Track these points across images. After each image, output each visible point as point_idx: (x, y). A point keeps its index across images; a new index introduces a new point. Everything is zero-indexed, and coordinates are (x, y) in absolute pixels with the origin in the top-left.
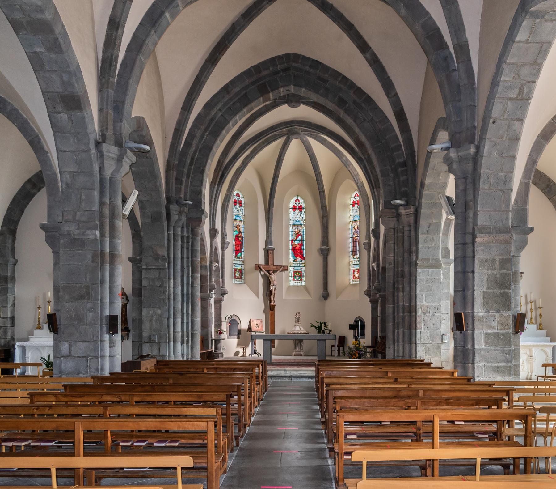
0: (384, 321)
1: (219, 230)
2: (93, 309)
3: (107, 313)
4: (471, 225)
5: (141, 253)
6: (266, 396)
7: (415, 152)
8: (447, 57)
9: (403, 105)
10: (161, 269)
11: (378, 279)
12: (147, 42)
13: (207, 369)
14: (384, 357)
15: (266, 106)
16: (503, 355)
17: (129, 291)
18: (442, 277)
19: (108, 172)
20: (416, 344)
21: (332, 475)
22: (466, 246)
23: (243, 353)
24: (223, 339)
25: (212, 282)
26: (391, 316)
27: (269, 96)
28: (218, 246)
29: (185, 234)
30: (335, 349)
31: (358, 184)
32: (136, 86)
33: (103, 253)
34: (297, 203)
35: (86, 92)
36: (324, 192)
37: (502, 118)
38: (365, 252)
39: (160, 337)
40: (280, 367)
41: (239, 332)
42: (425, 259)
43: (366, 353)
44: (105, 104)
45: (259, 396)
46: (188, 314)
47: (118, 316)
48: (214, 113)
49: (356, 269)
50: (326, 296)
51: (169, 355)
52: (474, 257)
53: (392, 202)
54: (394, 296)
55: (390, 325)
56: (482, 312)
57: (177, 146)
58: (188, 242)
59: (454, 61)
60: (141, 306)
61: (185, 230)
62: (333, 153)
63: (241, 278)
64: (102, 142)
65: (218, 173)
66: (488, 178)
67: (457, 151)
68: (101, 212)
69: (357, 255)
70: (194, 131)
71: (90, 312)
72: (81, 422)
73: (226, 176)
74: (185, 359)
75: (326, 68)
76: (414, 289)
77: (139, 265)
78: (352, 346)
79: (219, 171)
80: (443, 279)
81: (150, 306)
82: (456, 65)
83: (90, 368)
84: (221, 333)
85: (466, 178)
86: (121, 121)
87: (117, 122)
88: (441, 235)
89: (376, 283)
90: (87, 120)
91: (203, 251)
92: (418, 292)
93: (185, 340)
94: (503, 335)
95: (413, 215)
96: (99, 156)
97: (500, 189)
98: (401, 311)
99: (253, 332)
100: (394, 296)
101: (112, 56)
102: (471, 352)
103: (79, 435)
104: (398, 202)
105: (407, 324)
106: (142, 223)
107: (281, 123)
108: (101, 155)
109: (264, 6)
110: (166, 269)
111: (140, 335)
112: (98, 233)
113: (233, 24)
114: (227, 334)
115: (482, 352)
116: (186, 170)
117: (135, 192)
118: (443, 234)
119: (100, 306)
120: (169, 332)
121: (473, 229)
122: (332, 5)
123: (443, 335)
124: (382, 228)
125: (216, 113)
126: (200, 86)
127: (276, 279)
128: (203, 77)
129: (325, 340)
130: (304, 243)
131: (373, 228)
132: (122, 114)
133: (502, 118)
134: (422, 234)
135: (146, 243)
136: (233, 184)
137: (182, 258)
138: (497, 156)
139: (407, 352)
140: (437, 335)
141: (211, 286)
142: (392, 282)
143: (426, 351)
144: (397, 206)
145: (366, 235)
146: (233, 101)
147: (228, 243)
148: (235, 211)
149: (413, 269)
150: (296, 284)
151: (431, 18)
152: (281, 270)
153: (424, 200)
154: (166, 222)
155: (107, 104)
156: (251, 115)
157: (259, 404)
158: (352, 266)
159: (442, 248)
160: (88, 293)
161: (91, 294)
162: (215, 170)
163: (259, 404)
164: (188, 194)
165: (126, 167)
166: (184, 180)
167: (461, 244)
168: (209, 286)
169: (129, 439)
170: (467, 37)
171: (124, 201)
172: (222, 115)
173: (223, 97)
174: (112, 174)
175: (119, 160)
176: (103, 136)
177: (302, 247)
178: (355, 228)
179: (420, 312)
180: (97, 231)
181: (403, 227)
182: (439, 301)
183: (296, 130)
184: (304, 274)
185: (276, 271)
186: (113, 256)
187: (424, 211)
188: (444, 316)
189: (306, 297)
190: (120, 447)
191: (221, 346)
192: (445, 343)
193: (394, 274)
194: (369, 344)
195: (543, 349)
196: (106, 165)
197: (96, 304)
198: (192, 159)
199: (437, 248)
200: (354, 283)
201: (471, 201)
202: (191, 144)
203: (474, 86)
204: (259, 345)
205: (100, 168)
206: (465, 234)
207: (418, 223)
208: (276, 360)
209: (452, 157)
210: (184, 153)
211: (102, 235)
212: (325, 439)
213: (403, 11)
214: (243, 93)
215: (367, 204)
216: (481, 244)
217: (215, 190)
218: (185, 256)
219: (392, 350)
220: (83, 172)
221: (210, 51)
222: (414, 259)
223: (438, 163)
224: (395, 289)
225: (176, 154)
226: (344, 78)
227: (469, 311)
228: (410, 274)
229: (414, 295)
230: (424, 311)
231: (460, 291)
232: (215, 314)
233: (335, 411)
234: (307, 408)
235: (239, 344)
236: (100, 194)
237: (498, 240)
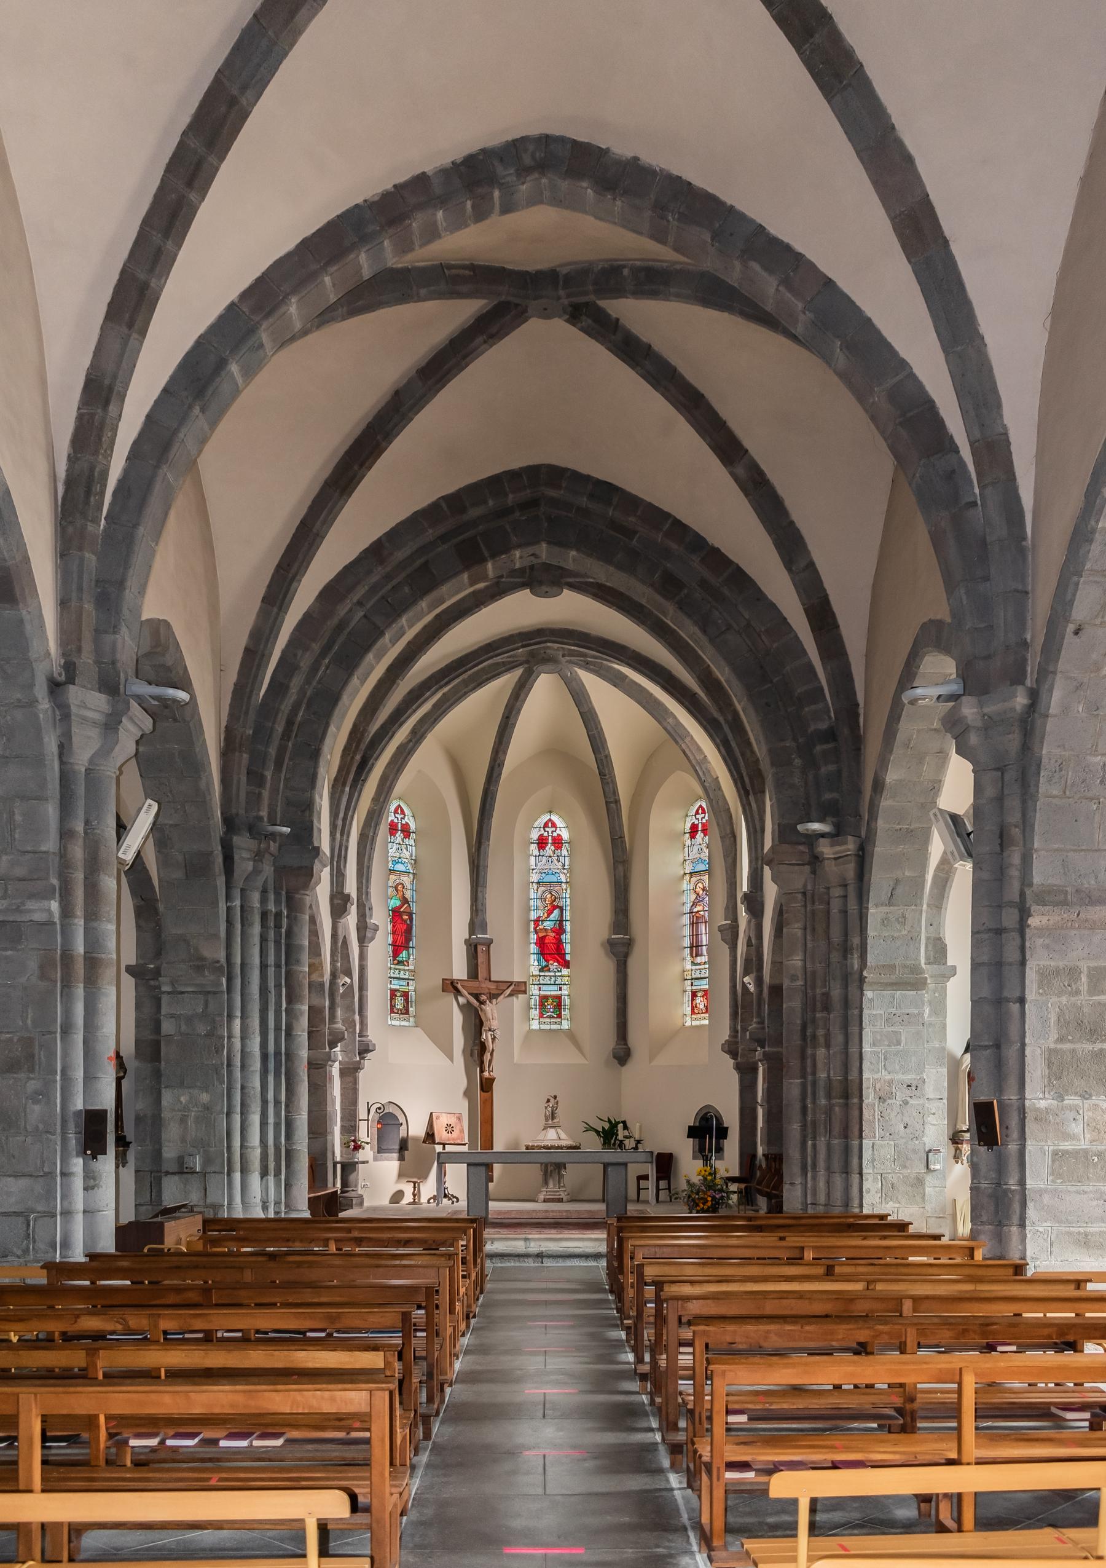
0: (775, 1117)
1: (354, 895)
2: (44, 1095)
3: (79, 1104)
4: (1016, 885)
5: (159, 953)
6: (482, 1306)
7: (858, 705)
8: (953, 472)
9: (828, 592)
10: (209, 992)
11: (759, 1015)
12: (181, 435)
13: (337, 1240)
14: (776, 1207)
15: (474, 593)
16: (1098, 1205)
17: (128, 1048)
18: (927, 1011)
19: (81, 758)
20: (861, 1174)
21: (685, 1517)
22: (1004, 936)
23: (414, 1195)
24: (363, 1163)
25: (337, 1023)
26: (797, 1106)
27: (486, 569)
28: (349, 934)
29: (271, 907)
30: (651, 1184)
31: (706, 784)
32: (153, 545)
33: (67, 958)
34: (550, 830)
35: (26, 560)
36: (617, 802)
37: (1098, 621)
38: (725, 949)
39: (207, 1161)
40: (512, 1231)
41: (403, 1145)
42: (884, 966)
43: (729, 1193)
44: (74, 587)
45: (469, 1306)
46: (277, 1102)
47: (105, 1111)
48: (345, 611)
49: (700, 990)
50: (622, 1055)
51: (230, 1204)
52: (1023, 963)
53: (799, 827)
54: (803, 1057)
55: (794, 1129)
56: (1044, 1098)
57: (251, 691)
58: (278, 926)
59: (971, 481)
60: (159, 1083)
61: (272, 897)
62: (644, 707)
63: (407, 1012)
64: (66, 683)
65: (353, 758)
66: (1061, 770)
67: (979, 701)
68: (63, 854)
69: (701, 955)
70: (295, 655)
71: (36, 1102)
72: (35, 1395)
73: (373, 764)
74: (271, 1215)
75: (631, 502)
76: (856, 1040)
77: (152, 983)
78: (696, 1179)
79: (355, 753)
80: (930, 1015)
81: (182, 1085)
82: (977, 491)
83: (34, 1242)
84: (357, 1148)
85: (1001, 770)
86: (115, 629)
87: (106, 632)
88: (925, 906)
89: (754, 1025)
90: (28, 627)
91: (315, 949)
92: (867, 1048)
93: (272, 1166)
95: (853, 858)
96: (58, 718)
97: (1090, 794)
98: (821, 1093)
99: (439, 1144)
100: (803, 1057)
101: (92, 469)
102: (1017, 1197)
103: (30, 1427)
104: (816, 826)
105: (837, 1128)
106: (160, 880)
107: (512, 636)
108: (63, 714)
109: (471, 353)
110: (223, 992)
111: (157, 1155)
112: (55, 906)
113: (397, 393)
114: (371, 1149)
115: (1046, 1199)
116: (272, 751)
117: (150, 805)
118: (928, 905)
119: (62, 1089)
120: (229, 1147)
121: (1022, 894)
122: (650, 346)
123: (930, 1151)
124: (771, 892)
125: (351, 610)
126: (311, 545)
127: (496, 1015)
128: (318, 523)
129: (625, 1165)
130: (568, 927)
131: (745, 888)
132: (118, 612)
133: (1098, 621)
134: (877, 906)
135: (172, 929)
136: (388, 784)
137: (264, 967)
138: (1084, 715)
139: (838, 1195)
140: (914, 1151)
141: (332, 1032)
142: (799, 1022)
143: (888, 1191)
144: (812, 839)
145: (727, 908)
146: (394, 582)
147: (376, 928)
148: (392, 850)
149: (853, 989)
150: (547, 1027)
151: (912, 376)
152: (508, 992)
153: (881, 824)
154: (223, 878)
155: (80, 589)
156: (438, 616)
157: (468, 1327)
158: (689, 982)
159: (928, 939)
160: (31, 1056)
161: (37, 1057)
162: (344, 751)
163: (468, 1327)
164: (279, 808)
165: (126, 744)
166: (268, 774)
167: (990, 930)
168: (330, 1034)
169: (155, 1430)
170: (1005, 422)
171: (122, 828)
172: (365, 616)
173: (369, 572)
174: (91, 761)
175: (111, 725)
176: (70, 668)
177: (563, 937)
178: (698, 889)
179: (872, 1096)
180: (52, 902)
181: (828, 888)
182: (920, 1068)
183: (548, 651)
184: (568, 1002)
185: (496, 996)
186: (93, 963)
187: (881, 850)
188: (933, 1106)
189: (569, 1057)
190: (129, 1451)
191: (357, 1180)
192: (935, 1171)
193: (805, 1005)
194: (735, 1172)
196: (75, 740)
197: (49, 1083)
198: (290, 723)
199: (914, 939)
200: (695, 1023)
201: (1016, 826)
202: (287, 687)
203: (1024, 543)
204: (457, 1177)
205: (61, 747)
206: (1000, 906)
207: (866, 879)
208: (500, 1212)
209: (966, 717)
210: (267, 710)
211: (67, 912)
212: (651, 1418)
213: (841, 359)
214: (419, 563)
215: (728, 831)
216: (1041, 931)
217: (345, 799)
218: (271, 960)
219: (798, 1191)
220: (17, 757)
221: (336, 460)
222: (856, 966)
223: (919, 731)
224: (807, 1039)
225: (247, 713)
226: (678, 523)
227: (1011, 1096)
228: (846, 1003)
229: (857, 1055)
230: (881, 1094)
231: (986, 1047)
232: (342, 1102)
234: (593, 1336)
235: (401, 1175)
236: (61, 811)
237: (1087, 920)
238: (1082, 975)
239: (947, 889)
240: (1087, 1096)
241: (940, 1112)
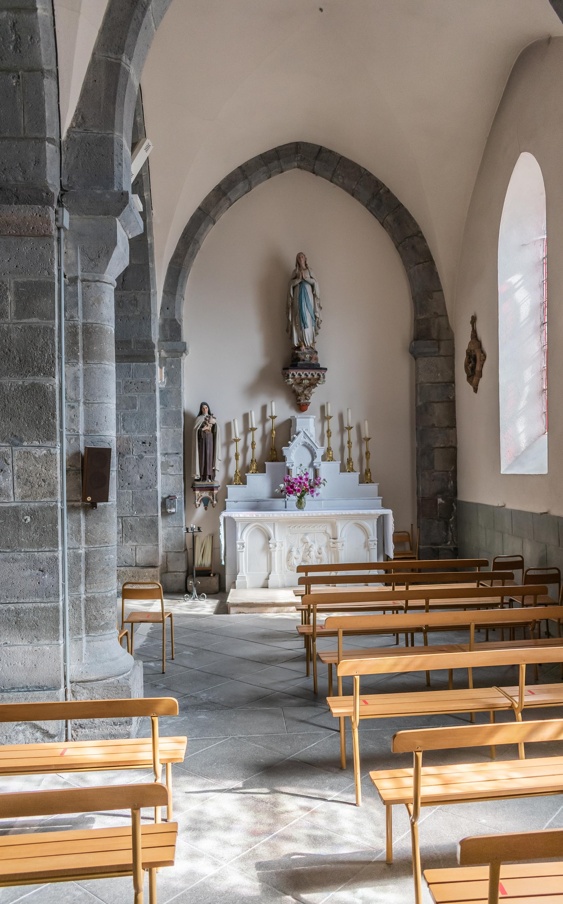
16: (31, 576)
94: (33, 513)
195: (359, 522)
238: (8, 293)
239: (180, 280)
240: (17, 442)
241: (177, 465)
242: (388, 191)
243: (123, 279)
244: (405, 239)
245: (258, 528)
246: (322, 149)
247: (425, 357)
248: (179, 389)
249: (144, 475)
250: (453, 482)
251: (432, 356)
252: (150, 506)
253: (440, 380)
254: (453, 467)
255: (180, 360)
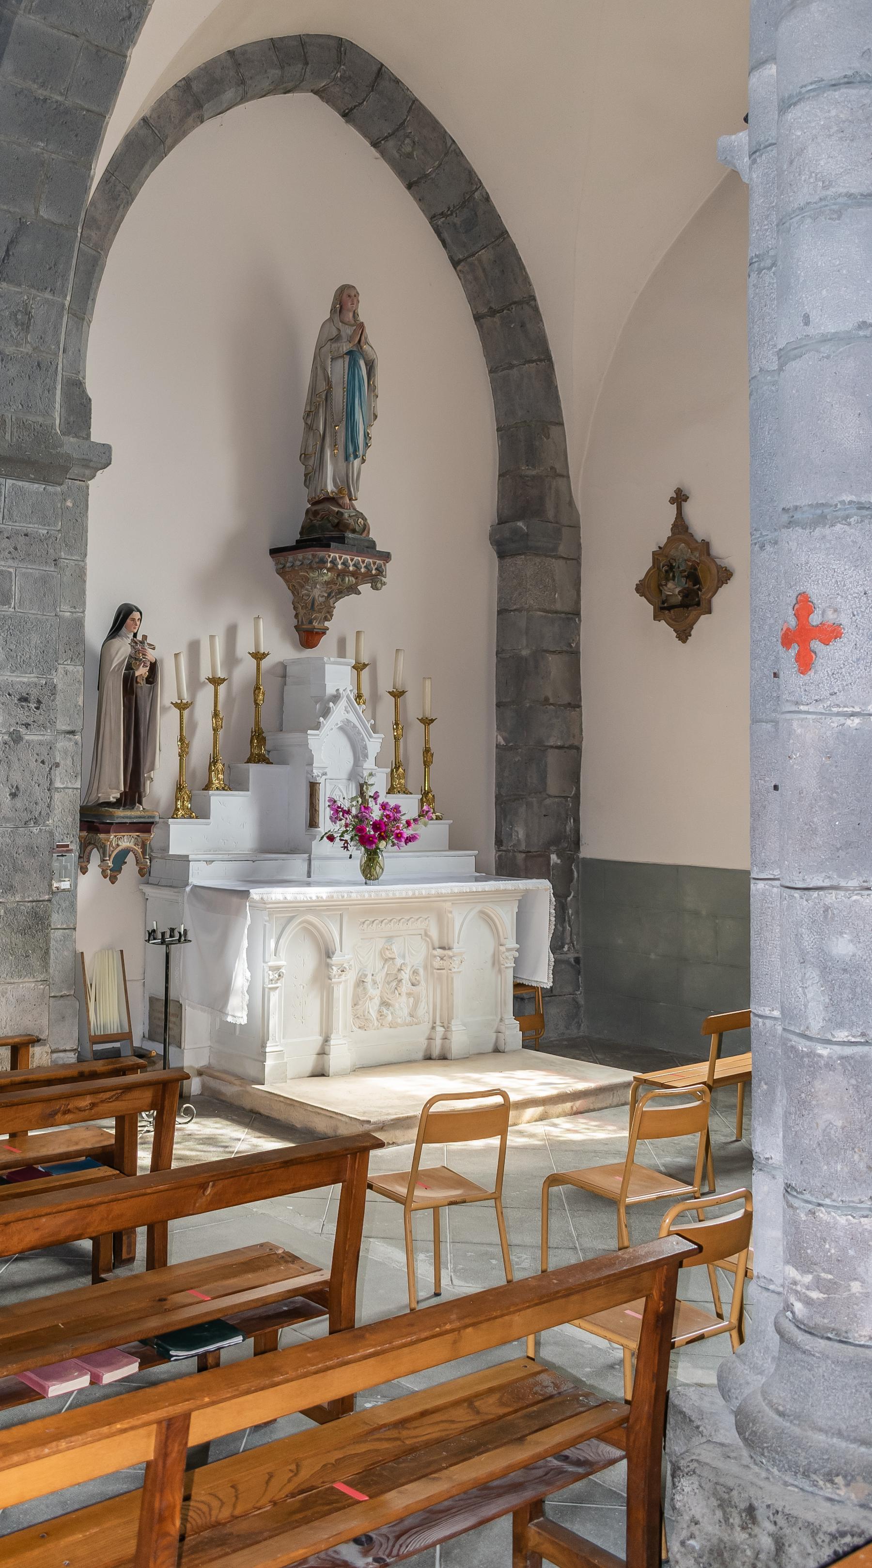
233: (849, 1478)
241: (69, 762)
242: (487, 199)
243: (7, 251)
244: (511, 304)
245: (305, 929)
246: (383, 68)
247: (537, 555)
248: (82, 564)
249: (22, 787)
250: (574, 819)
251: (547, 556)
252: (33, 872)
253: (558, 606)
254: (574, 788)
255: (88, 487)
